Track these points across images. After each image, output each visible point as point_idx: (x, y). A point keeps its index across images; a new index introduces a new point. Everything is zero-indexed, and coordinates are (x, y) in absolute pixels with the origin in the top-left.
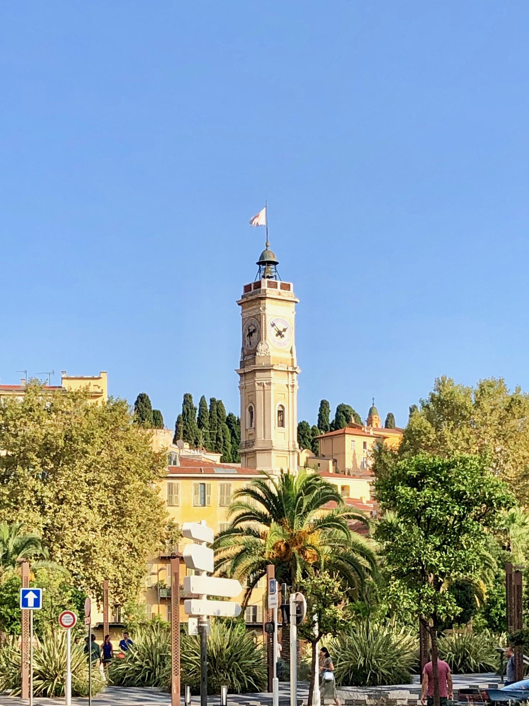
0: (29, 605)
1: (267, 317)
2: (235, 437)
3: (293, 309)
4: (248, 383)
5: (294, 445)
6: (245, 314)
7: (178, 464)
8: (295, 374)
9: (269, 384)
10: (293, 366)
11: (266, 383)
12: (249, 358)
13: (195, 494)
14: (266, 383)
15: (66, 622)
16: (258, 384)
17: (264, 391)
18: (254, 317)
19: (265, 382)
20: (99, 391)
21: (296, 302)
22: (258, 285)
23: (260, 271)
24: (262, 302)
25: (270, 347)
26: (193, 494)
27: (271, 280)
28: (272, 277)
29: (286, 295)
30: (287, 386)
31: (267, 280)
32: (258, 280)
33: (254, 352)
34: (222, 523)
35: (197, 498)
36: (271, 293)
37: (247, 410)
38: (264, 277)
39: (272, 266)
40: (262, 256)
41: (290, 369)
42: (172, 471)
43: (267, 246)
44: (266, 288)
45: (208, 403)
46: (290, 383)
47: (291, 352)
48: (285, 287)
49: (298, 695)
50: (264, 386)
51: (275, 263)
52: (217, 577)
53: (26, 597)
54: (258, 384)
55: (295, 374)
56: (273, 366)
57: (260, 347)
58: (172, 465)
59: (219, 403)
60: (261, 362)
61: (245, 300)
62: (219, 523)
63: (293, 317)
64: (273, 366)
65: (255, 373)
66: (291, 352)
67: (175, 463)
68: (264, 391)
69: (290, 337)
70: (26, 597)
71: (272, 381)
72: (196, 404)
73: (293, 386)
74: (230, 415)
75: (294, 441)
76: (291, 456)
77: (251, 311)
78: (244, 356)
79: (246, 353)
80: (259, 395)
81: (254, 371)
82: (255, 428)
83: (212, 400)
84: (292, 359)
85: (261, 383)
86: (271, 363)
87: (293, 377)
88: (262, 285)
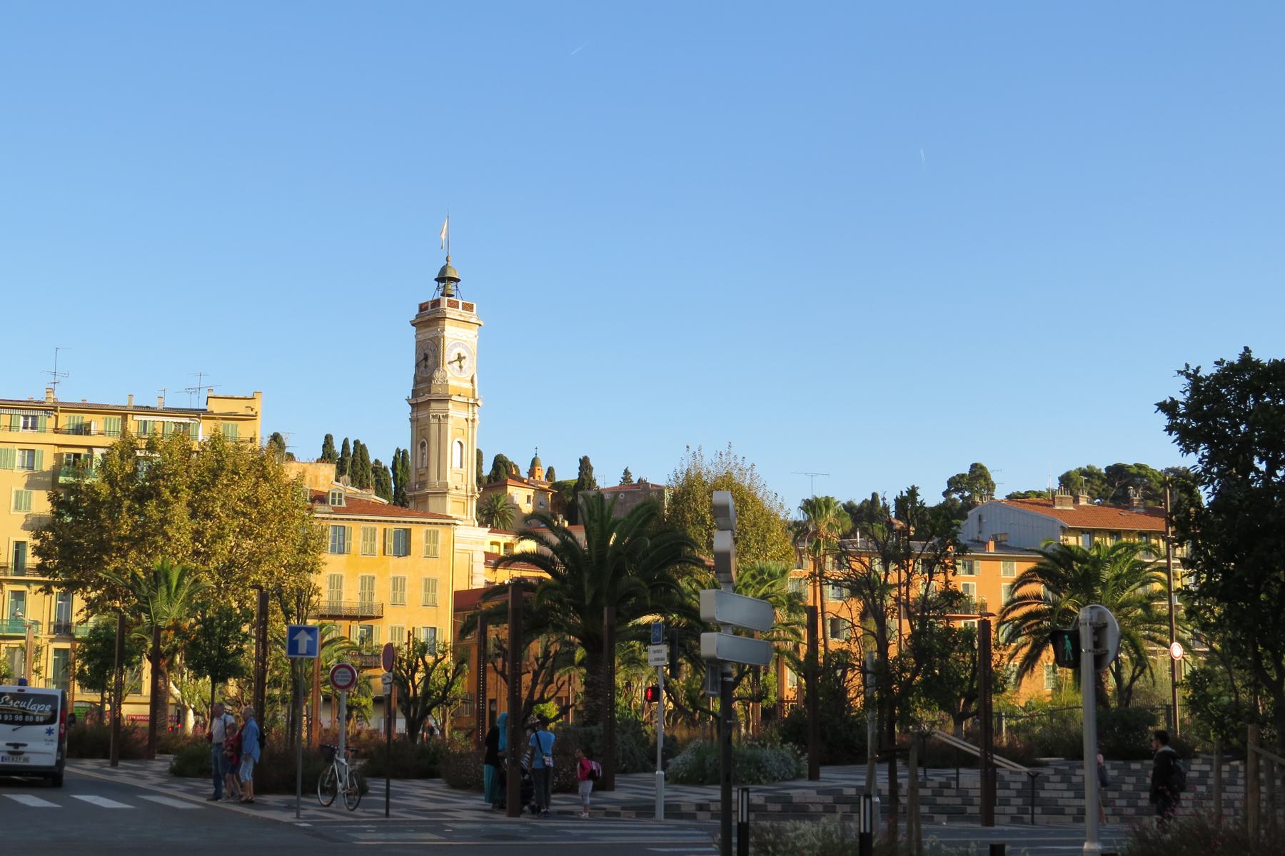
0: (300, 652)
1: (446, 343)
2: (382, 485)
3: (476, 333)
4: (422, 414)
5: (473, 490)
6: (419, 336)
7: (344, 504)
8: (476, 407)
9: (446, 417)
10: (474, 397)
11: (443, 416)
12: (422, 386)
13: (364, 540)
14: (443, 416)
15: (341, 680)
16: (433, 416)
17: (440, 424)
18: (430, 339)
19: (441, 415)
20: (253, 413)
21: (480, 325)
22: (436, 303)
23: (438, 288)
24: (441, 322)
25: (449, 374)
26: (361, 540)
27: (450, 298)
28: (452, 296)
29: (467, 315)
30: (467, 420)
31: (447, 298)
32: (436, 298)
33: (429, 380)
34: (394, 575)
35: (366, 545)
36: (451, 313)
37: (419, 446)
38: (442, 295)
39: (454, 284)
40: (444, 270)
41: (471, 401)
42: (337, 511)
43: (447, 261)
44: (446, 307)
45: (352, 446)
46: (471, 418)
47: (472, 381)
48: (468, 307)
49: (654, 796)
50: (439, 419)
51: (457, 280)
52: (699, 598)
53: (295, 638)
54: (433, 416)
55: (476, 407)
56: (451, 396)
57: (437, 374)
58: (337, 505)
59: (363, 447)
60: (436, 388)
61: (419, 320)
62: (392, 575)
63: (475, 340)
64: (451, 396)
65: (430, 404)
66: (472, 381)
67: (340, 502)
68: (440, 424)
69: (470, 365)
70: (295, 638)
71: (450, 413)
72: (338, 448)
73: (473, 421)
74: (377, 462)
75: (472, 485)
76: (469, 501)
77: (428, 333)
78: (417, 382)
79: (418, 378)
80: (434, 429)
81: (429, 402)
82: (427, 468)
83: (356, 443)
84: (474, 390)
85: (436, 416)
86: (450, 393)
87: (473, 411)
88: (442, 303)
